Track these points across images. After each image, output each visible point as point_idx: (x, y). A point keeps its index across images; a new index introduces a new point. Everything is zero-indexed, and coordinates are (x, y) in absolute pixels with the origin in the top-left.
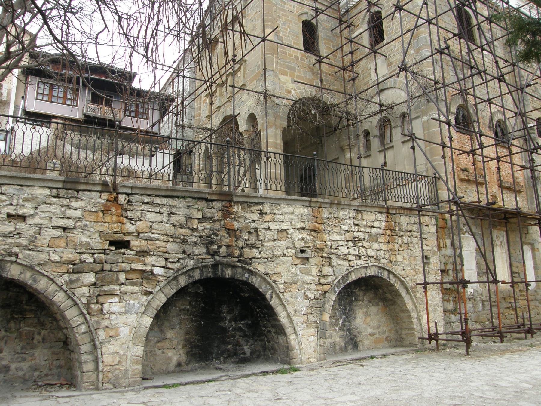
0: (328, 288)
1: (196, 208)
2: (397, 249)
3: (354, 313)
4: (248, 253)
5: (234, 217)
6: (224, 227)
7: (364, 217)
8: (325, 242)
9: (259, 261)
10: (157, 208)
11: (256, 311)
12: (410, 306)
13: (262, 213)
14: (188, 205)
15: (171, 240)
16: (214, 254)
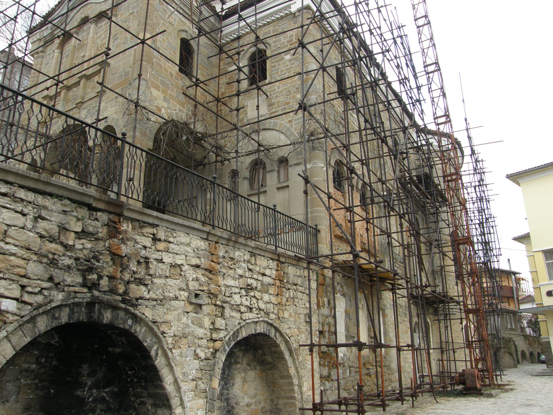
0: (220, 346)
1: (75, 216)
2: (284, 304)
3: (233, 378)
4: (138, 291)
5: (123, 239)
6: (109, 249)
7: (258, 262)
8: (219, 286)
9: (146, 303)
10: (19, 205)
11: (126, 374)
12: (292, 371)
13: (155, 239)
14: (65, 209)
15: (35, 258)
16: (94, 286)
